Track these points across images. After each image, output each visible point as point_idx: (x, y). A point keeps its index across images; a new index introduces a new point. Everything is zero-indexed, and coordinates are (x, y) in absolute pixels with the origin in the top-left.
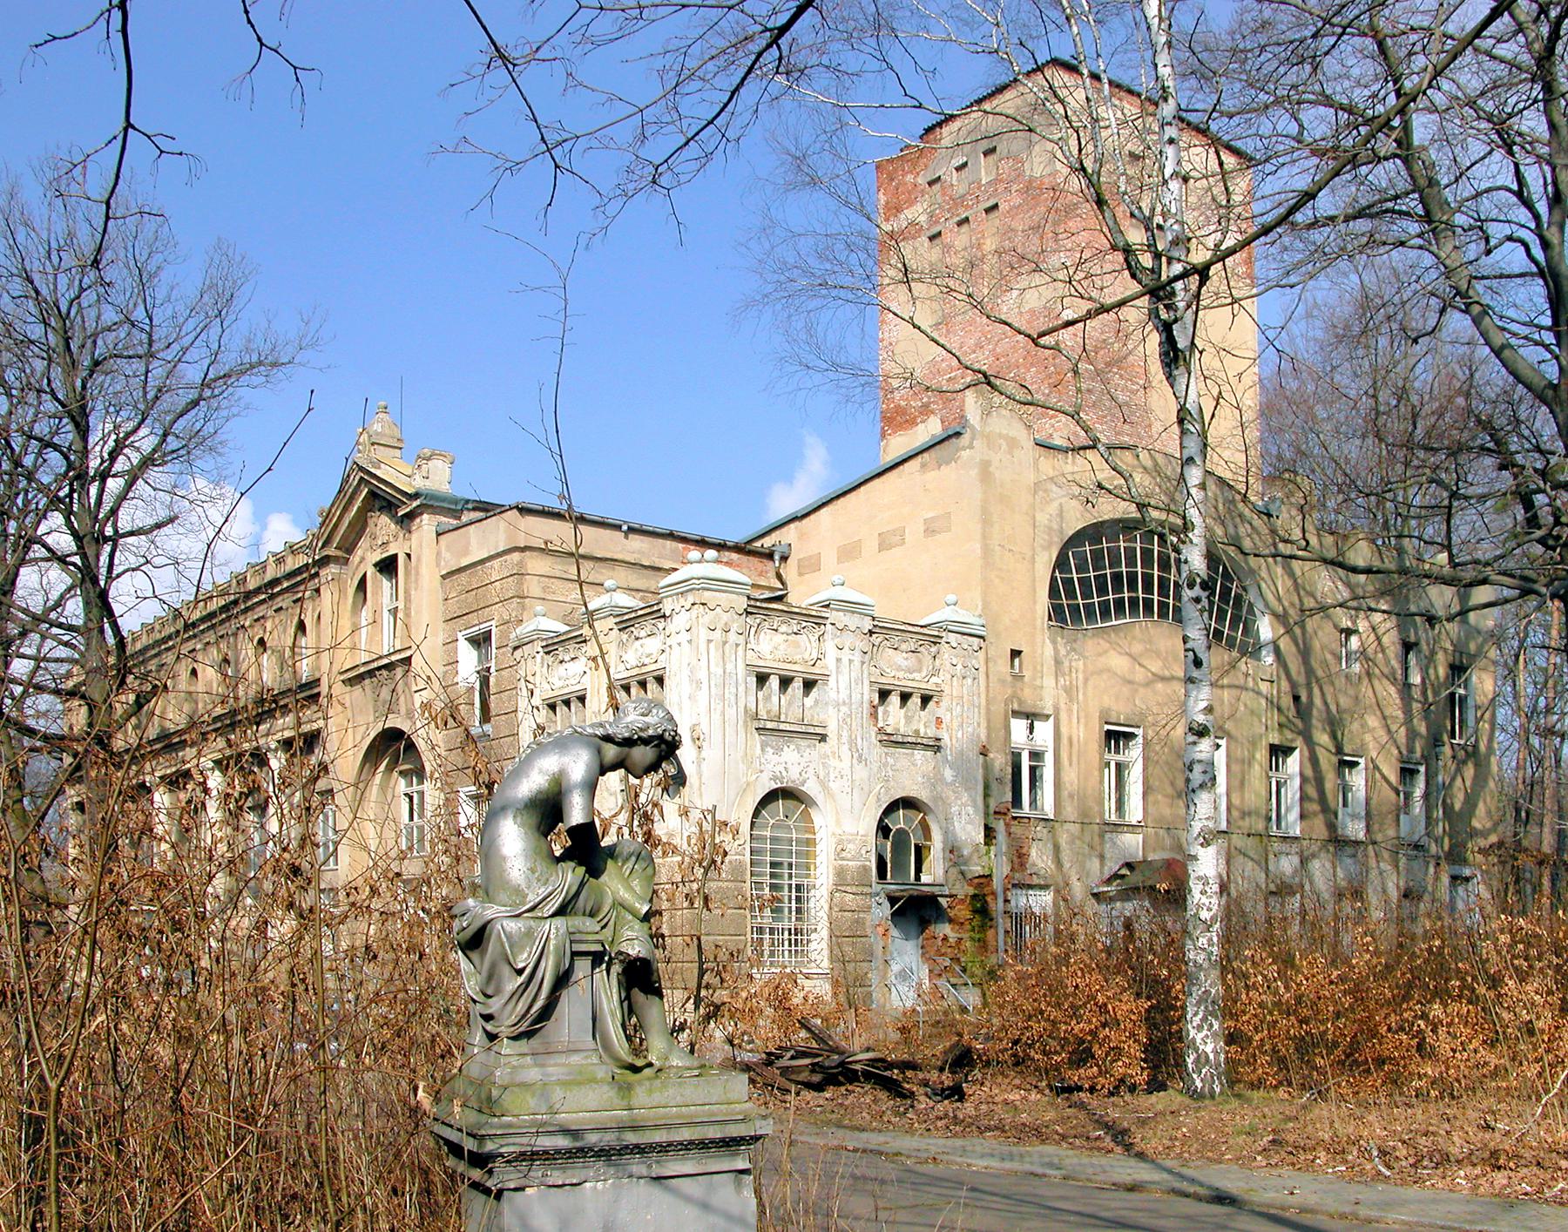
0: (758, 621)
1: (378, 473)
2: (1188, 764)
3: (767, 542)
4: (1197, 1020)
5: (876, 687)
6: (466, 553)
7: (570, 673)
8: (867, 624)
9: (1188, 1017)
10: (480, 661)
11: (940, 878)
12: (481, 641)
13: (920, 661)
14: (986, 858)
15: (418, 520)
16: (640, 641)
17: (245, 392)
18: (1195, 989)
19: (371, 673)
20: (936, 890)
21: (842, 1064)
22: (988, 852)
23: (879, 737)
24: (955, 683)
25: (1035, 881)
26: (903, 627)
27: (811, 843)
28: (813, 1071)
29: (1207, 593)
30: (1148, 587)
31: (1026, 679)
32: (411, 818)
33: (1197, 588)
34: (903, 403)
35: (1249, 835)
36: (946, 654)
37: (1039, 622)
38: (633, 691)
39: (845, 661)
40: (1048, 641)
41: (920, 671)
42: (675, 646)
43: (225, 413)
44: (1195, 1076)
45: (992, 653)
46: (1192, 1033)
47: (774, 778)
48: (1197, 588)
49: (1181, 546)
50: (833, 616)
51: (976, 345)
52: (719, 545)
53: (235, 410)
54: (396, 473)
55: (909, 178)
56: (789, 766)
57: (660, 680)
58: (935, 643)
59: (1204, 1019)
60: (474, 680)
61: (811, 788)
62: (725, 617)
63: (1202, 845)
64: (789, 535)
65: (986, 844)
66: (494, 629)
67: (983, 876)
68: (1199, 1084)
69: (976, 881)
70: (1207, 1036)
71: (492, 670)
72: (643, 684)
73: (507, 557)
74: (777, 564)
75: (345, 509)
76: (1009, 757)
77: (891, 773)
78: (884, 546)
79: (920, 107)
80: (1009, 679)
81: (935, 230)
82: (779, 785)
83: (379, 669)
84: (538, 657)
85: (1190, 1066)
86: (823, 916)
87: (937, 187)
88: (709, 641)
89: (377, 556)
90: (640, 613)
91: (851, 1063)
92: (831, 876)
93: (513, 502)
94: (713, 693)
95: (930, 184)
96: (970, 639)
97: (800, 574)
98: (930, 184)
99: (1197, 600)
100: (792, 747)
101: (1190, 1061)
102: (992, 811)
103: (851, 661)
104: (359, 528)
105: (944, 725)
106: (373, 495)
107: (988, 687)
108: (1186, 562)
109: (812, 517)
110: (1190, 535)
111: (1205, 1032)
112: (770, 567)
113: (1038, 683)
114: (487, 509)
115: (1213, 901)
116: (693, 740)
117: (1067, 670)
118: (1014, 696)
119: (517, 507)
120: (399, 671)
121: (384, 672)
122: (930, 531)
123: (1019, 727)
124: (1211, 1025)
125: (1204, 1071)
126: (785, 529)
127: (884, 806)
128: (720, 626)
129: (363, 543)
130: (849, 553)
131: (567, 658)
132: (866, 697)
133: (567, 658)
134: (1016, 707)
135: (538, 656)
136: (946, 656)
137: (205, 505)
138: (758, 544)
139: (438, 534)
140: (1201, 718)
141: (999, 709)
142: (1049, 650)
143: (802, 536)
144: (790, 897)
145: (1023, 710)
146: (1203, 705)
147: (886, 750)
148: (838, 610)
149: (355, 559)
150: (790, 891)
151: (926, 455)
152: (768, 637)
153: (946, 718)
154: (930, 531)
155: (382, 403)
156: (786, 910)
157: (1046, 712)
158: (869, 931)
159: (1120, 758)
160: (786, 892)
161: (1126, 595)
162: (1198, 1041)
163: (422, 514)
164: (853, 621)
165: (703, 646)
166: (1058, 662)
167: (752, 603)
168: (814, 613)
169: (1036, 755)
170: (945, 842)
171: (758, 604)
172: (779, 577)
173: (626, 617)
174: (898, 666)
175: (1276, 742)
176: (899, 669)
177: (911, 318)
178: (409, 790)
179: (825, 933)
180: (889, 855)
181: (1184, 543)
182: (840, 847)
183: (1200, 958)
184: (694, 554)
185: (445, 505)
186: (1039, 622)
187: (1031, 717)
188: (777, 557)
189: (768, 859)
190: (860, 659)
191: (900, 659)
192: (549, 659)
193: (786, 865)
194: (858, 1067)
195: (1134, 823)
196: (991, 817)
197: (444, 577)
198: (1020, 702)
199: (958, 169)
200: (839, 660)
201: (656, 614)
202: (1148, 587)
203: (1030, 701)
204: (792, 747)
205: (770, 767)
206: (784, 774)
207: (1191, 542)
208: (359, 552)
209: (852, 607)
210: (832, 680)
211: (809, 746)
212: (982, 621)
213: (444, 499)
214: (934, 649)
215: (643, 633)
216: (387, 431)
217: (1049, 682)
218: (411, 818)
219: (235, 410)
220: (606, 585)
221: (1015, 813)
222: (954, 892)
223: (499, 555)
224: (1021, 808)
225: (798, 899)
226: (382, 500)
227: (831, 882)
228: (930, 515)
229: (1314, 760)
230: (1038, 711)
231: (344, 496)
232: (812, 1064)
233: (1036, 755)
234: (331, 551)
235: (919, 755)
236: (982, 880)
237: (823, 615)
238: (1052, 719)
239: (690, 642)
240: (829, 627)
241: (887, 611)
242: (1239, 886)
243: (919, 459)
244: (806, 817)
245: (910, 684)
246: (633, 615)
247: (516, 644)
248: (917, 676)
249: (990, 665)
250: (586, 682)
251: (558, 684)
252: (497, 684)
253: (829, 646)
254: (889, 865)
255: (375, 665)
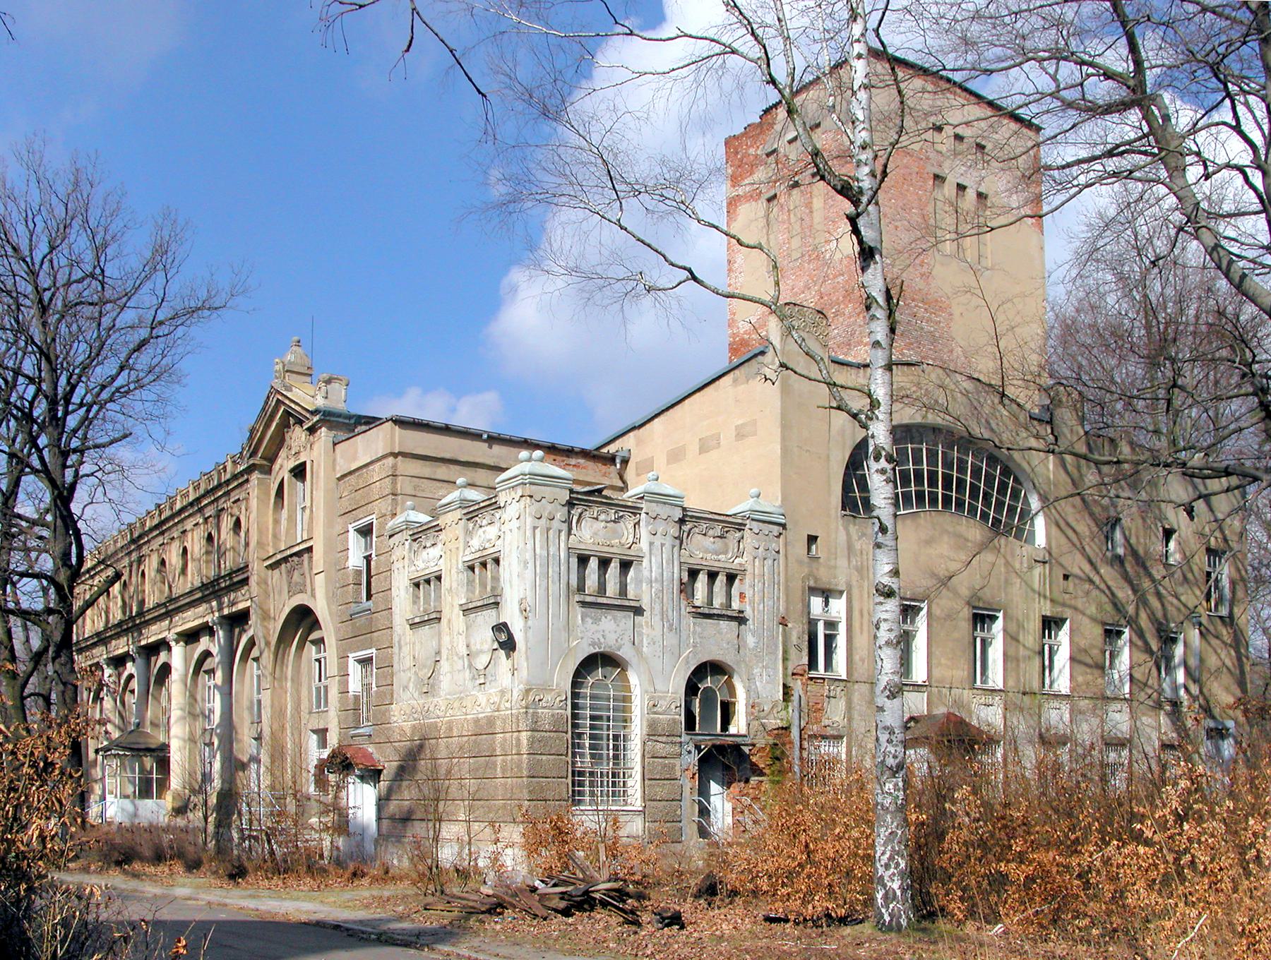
0: (579, 511)
1: (289, 394)
2: (875, 622)
3: (612, 449)
4: (885, 858)
5: (685, 567)
6: (355, 459)
7: (431, 556)
8: (678, 514)
9: (877, 856)
10: (366, 549)
11: (743, 731)
12: (366, 531)
13: (726, 545)
14: (784, 713)
15: (319, 432)
16: (483, 529)
17: (197, 331)
18: (883, 830)
19: (285, 560)
20: (739, 740)
21: (587, 893)
22: (787, 707)
23: (688, 610)
24: (757, 564)
25: (830, 732)
26: (710, 516)
27: (627, 699)
28: (562, 899)
29: (892, 466)
30: (933, 483)
31: (821, 560)
32: (320, 680)
33: (883, 460)
34: (746, 337)
35: (1024, 694)
36: (749, 540)
37: (833, 512)
38: (477, 570)
39: (657, 543)
40: (841, 528)
41: (726, 553)
42: (508, 533)
43: (180, 350)
44: (883, 910)
45: (790, 538)
46: (881, 871)
47: (593, 644)
48: (883, 460)
49: (869, 422)
50: (644, 505)
51: (805, 287)
52: (568, 450)
53: (189, 348)
54: (305, 396)
55: (752, 151)
56: (607, 632)
57: (497, 561)
58: (740, 530)
59: (891, 858)
60: (362, 564)
61: (625, 652)
62: (550, 507)
63: (888, 697)
64: (628, 442)
65: (784, 700)
66: (375, 521)
67: (782, 728)
68: (887, 918)
69: (776, 732)
70: (894, 874)
71: (373, 556)
72: (484, 565)
73: (384, 461)
74: (618, 466)
75: (267, 426)
76: (806, 627)
77: (698, 640)
78: (704, 448)
79: (631, 34)
80: (806, 560)
81: (772, 193)
82: (597, 650)
83: (291, 556)
84: (407, 543)
85: (879, 901)
86: (638, 759)
87: (772, 158)
88: (535, 528)
89: (292, 464)
90: (482, 505)
91: (593, 892)
92: (644, 728)
93: (388, 416)
94: (538, 571)
95: (768, 155)
96: (771, 526)
97: (638, 475)
98: (768, 155)
99: (883, 471)
100: (609, 617)
101: (879, 895)
102: (790, 672)
103: (662, 545)
104: (279, 441)
105: (747, 600)
106: (287, 414)
107: (787, 566)
108: (873, 437)
109: (648, 426)
110: (876, 412)
111: (892, 870)
112: (613, 470)
113: (832, 563)
114: (371, 422)
115: (898, 749)
116: (521, 612)
117: (858, 553)
118: (810, 575)
119: (391, 419)
120: (306, 556)
121: (295, 559)
122: (740, 435)
123: (817, 603)
124: (898, 864)
125: (891, 906)
126: (625, 438)
127: (693, 668)
128: (545, 514)
129: (283, 453)
130: (675, 456)
131: (428, 545)
132: (676, 576)
133: (428, 545)
134: (812, 583)
135: (407, 543)
136: (749, 540)
137: (146, 422)
138: (605, 450)
139: (335, 444)
140: (886, 580)
141: (797, 585)
142: (842, 536)
143: (639, 442)
144: (608, 745)
145: (818, 586)
146: (888, 568)
147: (695, 620)
148: (651, 501)
149: (276, 467)
150: (608, 740)
151: (737, 372)
152: (589, 524)
153: (749, 594)
154: (740, 435)
155: (296, 338)
156: (605, 756)
157: (840, 588)
158: (678, 774)
159: (984, 635)
160: (605, 742)
161: (913, 489)
162: (886, 878)
163: (320, 428)
164: (664, 511)
165: (529, 533)
166: (850, 547)
167: (574, 495)
168: (630, 504)
169: (831, 625)
170: (748, 697)
171: (580, 496)
172: (621, 478)
173: (472, 509)
174: (703, 550)
175: (1048, 614)
176: (707, 551)
177: (619, 220)
178: (318, 656)
179: (638, 777)
180: (698, 710)
181: (871, 419)
182: (651, 703)
183: (888, 801)
184: (524, 454)
185: (340, 420)
186: (833, 512)
187: (827, 594)
188: (618, 461)
189: (588, 712)
190: (671, 543)
191: (708, 542)
192: (415, 545)
193: (605, 718)
194: (597, 896)
195: (920, 683)
196: (790, 679)
197: (339, 479)
198: (816, 580)
199: (790, 142)
200: (651, 544)
201: (494, 506)
202: (933, 483)
203: (825, 579)
204: (609, 617)
205: (590, 634)
206: (602, 640)
207: (877, 418)
208: (279, 461)
209: (663, 499)
210: (645, 562)
211: (625, 617)
212: (782, 511)
213: (339, 415)
214: (738, 535)
215: (485, 522)
216: (299, 361)
217: (842, 562)
218: (320, 680)
219: (189, 348)
220: (458, 482)
221: (813, 674)
222: (755, 741)
223: (378, 460)
224: (816, 669)
225: (616, 748)
226: (291, 418)
227: (644, 732)
228: (740, 422)
229: (1141, 634)
230: (832, 587)
231: (266, 416)
232: (562, 893)
233: (831, 625)
234: (257, 460)
235: (724, 624)
236: (780, 732)
237: (639, 505)
238: (845, 595)
239: (519, 528)
240: (643, 515)
241: (694, 502)
242: (274, 727)
243: (731, 375)
244: (623, 677)
245: (716, 564)
246: (476, 507)
247: (392, 532)
248: (722, 557)
249: (789, 548)
250: (442, 565)
251: (422, 566)
252: (377, 568)
253: (644, 532)
254: (697, 719)
255: (288, 552)
